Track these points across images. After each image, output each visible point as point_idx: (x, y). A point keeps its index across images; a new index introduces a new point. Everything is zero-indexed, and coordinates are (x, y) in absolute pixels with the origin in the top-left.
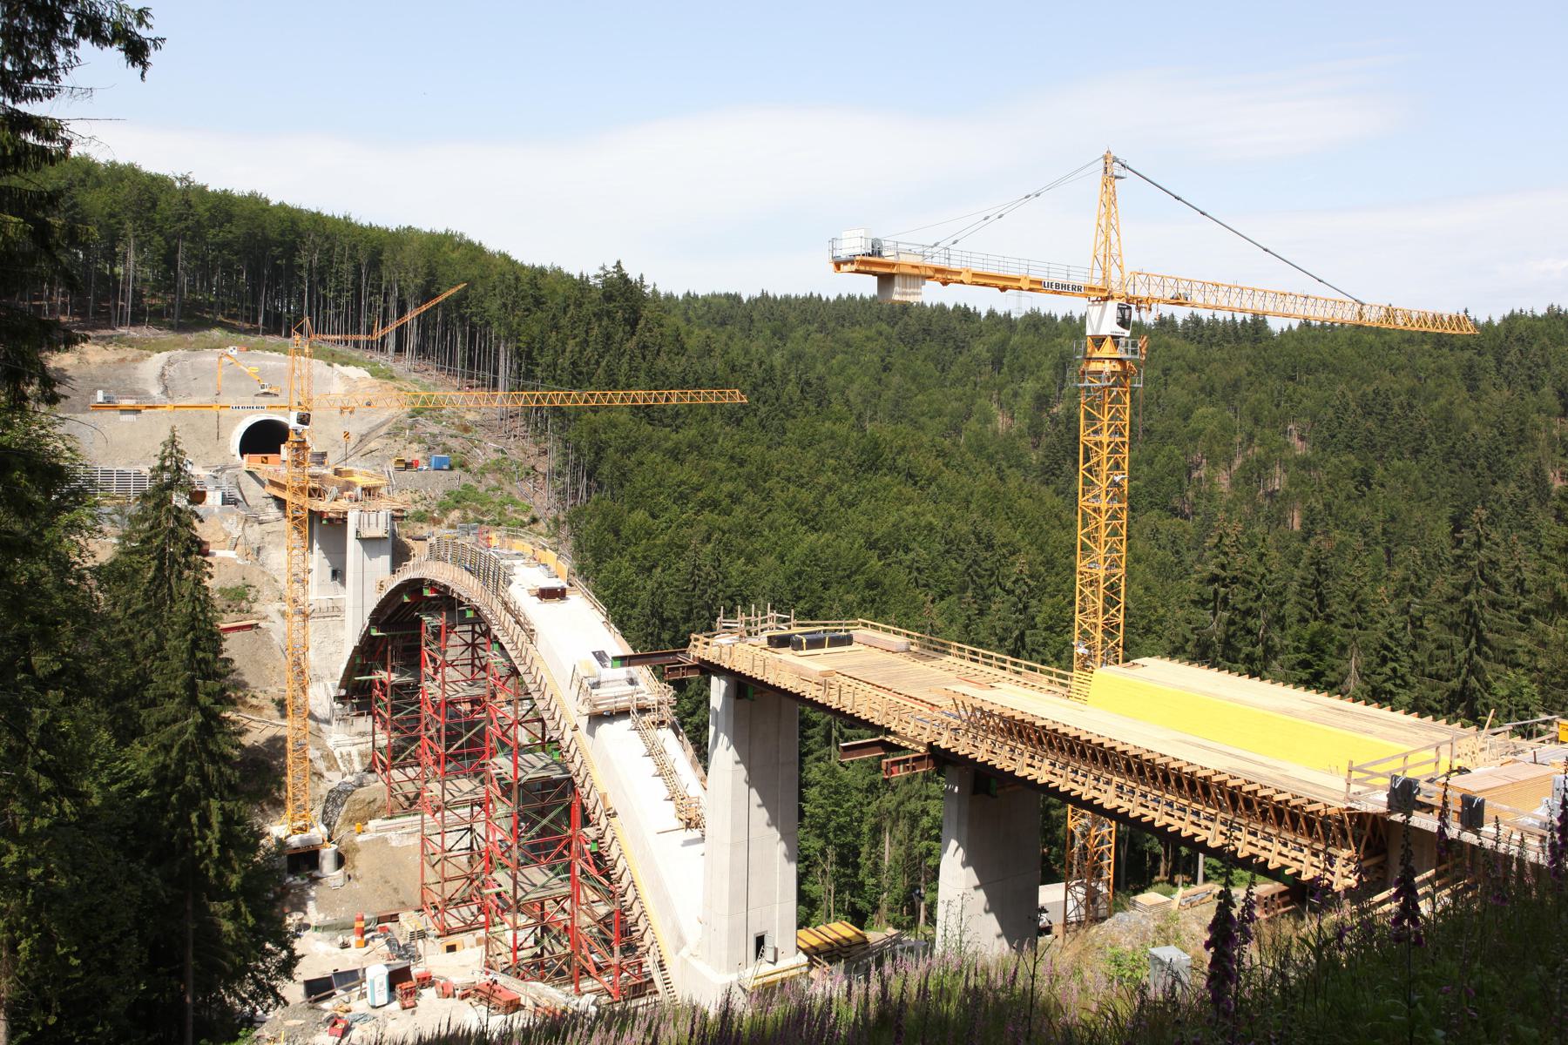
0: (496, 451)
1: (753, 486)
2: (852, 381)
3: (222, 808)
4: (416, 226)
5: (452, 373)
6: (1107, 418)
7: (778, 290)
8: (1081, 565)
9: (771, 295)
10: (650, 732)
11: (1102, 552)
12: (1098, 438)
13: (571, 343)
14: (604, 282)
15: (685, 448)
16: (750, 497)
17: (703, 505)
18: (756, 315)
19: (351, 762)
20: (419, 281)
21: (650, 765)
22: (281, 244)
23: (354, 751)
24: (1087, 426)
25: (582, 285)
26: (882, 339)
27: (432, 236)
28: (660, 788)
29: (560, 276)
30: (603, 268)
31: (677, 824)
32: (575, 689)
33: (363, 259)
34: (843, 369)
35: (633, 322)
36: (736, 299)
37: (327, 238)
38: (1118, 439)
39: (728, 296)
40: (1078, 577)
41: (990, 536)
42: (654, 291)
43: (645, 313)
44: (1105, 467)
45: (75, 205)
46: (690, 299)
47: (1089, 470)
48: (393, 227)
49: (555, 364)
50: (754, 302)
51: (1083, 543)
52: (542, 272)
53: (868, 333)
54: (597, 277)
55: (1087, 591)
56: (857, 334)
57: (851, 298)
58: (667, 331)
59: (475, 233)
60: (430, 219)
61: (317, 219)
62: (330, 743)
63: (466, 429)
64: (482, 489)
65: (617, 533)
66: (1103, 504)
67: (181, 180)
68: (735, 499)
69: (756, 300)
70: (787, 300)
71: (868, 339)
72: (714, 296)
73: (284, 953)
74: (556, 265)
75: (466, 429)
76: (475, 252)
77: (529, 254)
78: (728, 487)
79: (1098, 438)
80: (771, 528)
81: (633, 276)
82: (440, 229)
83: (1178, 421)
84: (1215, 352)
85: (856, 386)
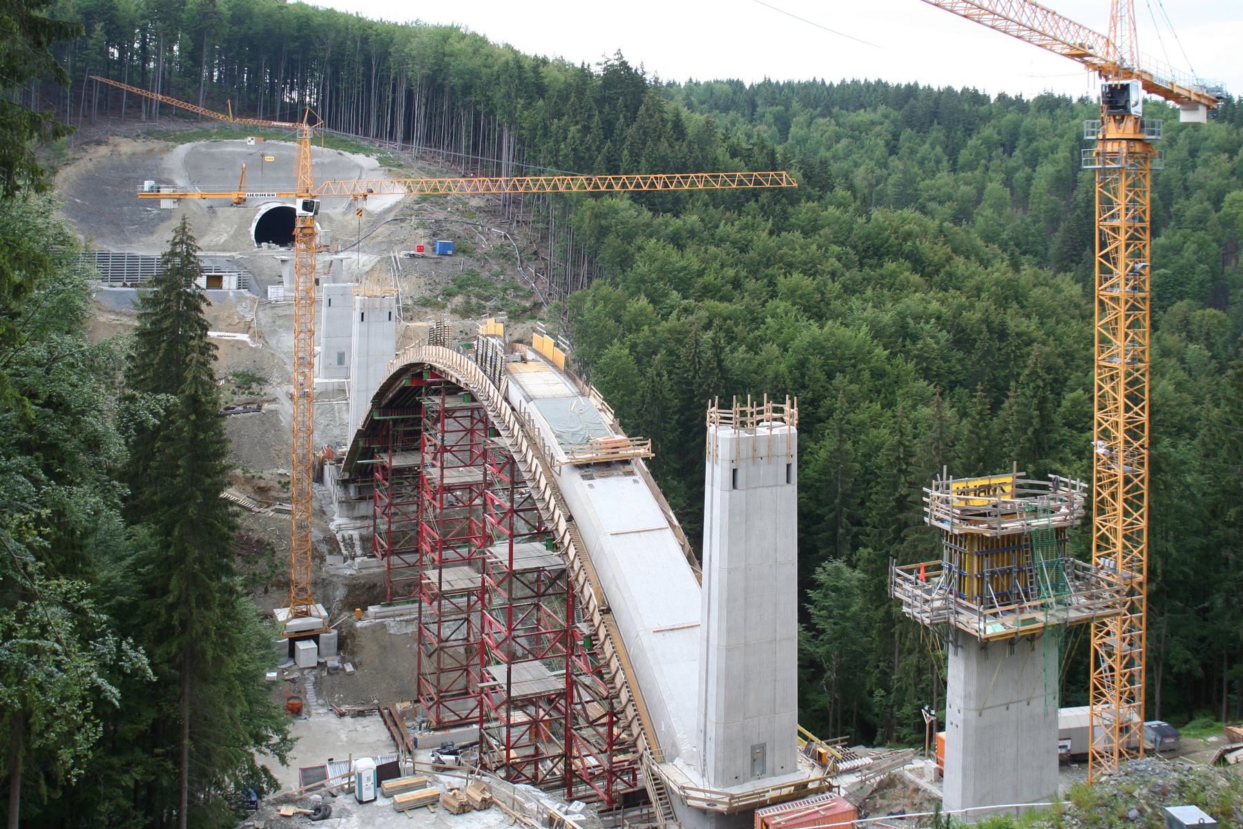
8: (1099, 359)
9: (774, 81)
15: (684, 234)
19: (352, 546)
20: (425, 71)
36: (737, 85)
38: (1138, 225)
39: (730, 82)
43: (646, 99)
46: (692, 86)
50: (757, 90)
56: (863, 116)
65: (618, 320)
68: (736, 284)
72: (716, 82)
78: (731, 272)
81: (633, 64)
85: (862, 169)
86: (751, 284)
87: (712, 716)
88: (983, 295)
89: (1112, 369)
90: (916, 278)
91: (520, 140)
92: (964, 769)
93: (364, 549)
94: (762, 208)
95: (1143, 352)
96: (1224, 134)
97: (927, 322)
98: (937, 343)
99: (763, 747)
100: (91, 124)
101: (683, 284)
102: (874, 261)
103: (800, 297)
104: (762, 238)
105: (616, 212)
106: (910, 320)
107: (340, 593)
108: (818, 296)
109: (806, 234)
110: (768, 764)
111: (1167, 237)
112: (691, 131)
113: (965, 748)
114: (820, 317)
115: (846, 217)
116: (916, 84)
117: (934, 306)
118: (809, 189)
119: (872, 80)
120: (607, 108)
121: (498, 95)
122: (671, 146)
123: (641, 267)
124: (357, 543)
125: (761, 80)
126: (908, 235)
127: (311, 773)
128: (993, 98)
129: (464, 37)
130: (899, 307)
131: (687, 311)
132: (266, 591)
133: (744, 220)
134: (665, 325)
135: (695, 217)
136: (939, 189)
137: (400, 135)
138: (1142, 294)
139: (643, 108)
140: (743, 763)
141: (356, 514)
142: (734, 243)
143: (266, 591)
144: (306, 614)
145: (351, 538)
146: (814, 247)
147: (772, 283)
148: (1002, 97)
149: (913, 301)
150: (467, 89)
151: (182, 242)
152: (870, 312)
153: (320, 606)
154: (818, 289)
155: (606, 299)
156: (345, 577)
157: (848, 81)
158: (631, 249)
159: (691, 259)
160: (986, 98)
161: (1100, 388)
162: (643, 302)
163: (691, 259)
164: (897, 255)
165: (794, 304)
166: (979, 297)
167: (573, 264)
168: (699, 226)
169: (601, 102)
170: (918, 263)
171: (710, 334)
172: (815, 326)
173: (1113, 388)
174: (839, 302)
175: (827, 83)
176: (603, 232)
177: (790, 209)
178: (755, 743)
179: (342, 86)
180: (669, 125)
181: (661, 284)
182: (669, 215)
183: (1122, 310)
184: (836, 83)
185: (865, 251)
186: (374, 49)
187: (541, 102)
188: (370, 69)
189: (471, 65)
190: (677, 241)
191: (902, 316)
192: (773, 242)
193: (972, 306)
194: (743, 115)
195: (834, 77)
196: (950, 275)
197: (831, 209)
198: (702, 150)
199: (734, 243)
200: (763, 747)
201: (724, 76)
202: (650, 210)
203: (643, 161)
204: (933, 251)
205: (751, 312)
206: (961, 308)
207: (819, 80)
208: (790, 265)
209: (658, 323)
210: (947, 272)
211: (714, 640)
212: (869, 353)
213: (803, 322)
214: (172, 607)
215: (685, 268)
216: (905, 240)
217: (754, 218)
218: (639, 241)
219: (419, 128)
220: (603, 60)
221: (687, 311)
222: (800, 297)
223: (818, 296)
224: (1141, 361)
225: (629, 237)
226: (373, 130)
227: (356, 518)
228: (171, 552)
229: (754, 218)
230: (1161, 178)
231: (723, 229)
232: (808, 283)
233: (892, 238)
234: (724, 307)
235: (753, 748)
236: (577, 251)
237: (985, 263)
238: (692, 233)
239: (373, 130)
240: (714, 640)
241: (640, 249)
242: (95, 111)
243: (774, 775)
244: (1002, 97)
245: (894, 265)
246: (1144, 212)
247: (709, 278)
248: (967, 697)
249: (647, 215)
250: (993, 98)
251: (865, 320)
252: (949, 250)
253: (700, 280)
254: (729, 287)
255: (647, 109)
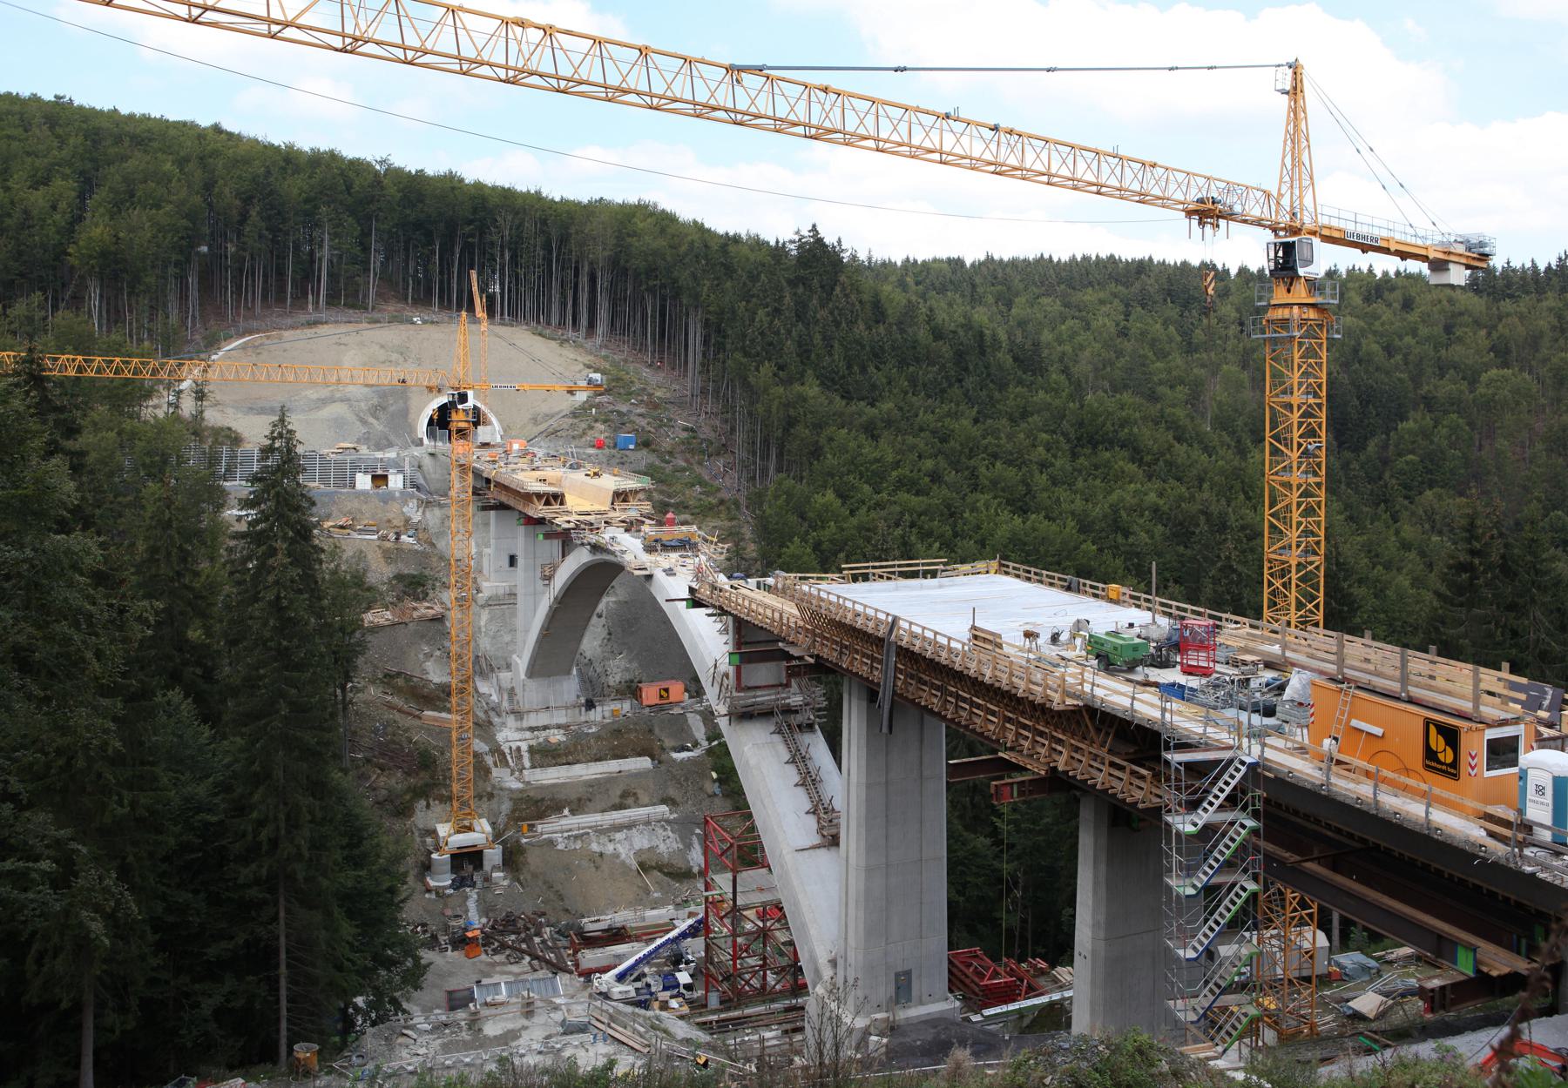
0: (686, 429)
1: (956, 465)
2: (1082, 348)
3: (1341, 916)
4: (608, 197)
5: (643, 349)
6: (1297, 374)
7: (1004, 253)
8: (1269, 551)
9: (996, 257)
10: (798, 736)
11: (1293, 535)
12: (1286, 399)
13: (761, 313)
14: (799, 248)
15: (880, 425)
16: (951, 477)
17: (901, 484)
18: (978, 280)
19: (520, 757)
20: (607, 253)
21: (792, 774)
22: (470, 222)
23: (524, 746)
24: (1274, 386)
25: (779, 251)
26: (1116, 302)
27: (623, 206)
28: (802, 801)
29: (758, 244)
30: (797, 233)
31: (817, 840)
32: (717, 686)
33: (554, 233)
34: (1072, 337)
35: (828, 289)
36: (957, 264)
37: (517, 213)
38: (1311, 401)
39: (949, 261)
40: (1266, 565)
41: (1223, 516)
42: (854, 258)
43: (843, 278)
44: (1296, 434)
45: (271, 193)
46: (909, 265)
47: (1276, 438)
48: (585, 201)
49: (744, 336)
50: (978, 267)
51: (1272, 526)
52: (736, 239)
53: (1102, 295)
54: (792, 242)
55: (1278, 584)
56: (1089, 296)
57: (1086, 259)
58: (865, 297)
59: (666, 202)
60: (622, 192)
61: (507, 194)
62: (500, 737)
63: (656, 407)
64: (669, 468)
65: (803, 517)
66: (1296, 477)
67: (381, 163)
68: (935, 477)
69: (981, 264)
70: (1014, 263)
71: (1102, 302)
72: (935, 260)
73: (409, 963)
74: (753, 233)
75: (656, 407)
76: (665, 221)
77: (722, 222)
78: (929, 464)
79: (1286, 399)
80: (972, 511)
81: (829, 239)
82: (632, 199)
83: (1464, 386)
84: (1507, 305)
85: (1087, 353)
86: (951, 477)
87: (852, 942)
88: (1206, 486)
89: (1283, 562)
90: (1132, 468)
91: (707, 324)
92: (1092, 1003)
93: (532, 759)
94: (966, 395)
95: (1318, 543)
96: (1483, 308)
97: (1142, 516)
98: (1152, 537)
99: (908, 973)
100: (254, 317)
101: (877, 479)
102: (1087, 451)
103: (1003, 490)
104: (964, 425)
105: (805, 400)
106: (1123, 514)
107: (506, 807)
108: (1022, 489)
109: (1012, 420)
110: (915, 993)
111: (1415, 421)
112: (892, 313)
113: (1093, 983)
114: (1024, 511)
115: (1057, 402)
116: (1150, 259)
117: (1152, 497)
118: (1019, 373)
119: (1103, 255)
120: (800, 290)
121: (684, 277)
122: (869, 328)
123: (830, 460)
124: (526, 756)
125: (982, 258)
126: (1124, 423)
127: (458, 995)
128: (1233, 272)
129: (652, 214)
130: (1114, 497)
131: (879, 505)
132: (428, 806)
133: (946, 408)
134: (854, 521)
135: (891, 405)
136: (1169, 372)
137: (584, 321)
138: (1318, 480)
139: (838, 289)
140: (885, 990)
141: (525, 724)
142: (933, 432)
143: (428, 806)
144: (470, 829)
145: (519, 749)
146: (1022, 436)
147: (974, 475)
148: (1243, 271)
149: (1125, 494)
150: (651, 271)
151: (281, 436)
152: (1079, 504)
153: (484, 822)
154: (1024, 482)
155: (789, 494)
156: (510, 790)
157: (1046, 256)
158: (822, 441)
159: (886, 449)
160: (1226, 272)
161: (1270, 584)
162: (830, 495)
163: (886, 449)
164: (1110, 443)
165: (995, 497)
166: (1200, 488)
167: (762, 458)
168: (897, 414)
169: (792, 283)
170: (1136, 453)
171: (898, 532)
172: (1018, 520)
173: (1284, 585)
174: (1045, 495)
175: (1055, 260)
176: (791, 423)
177: (997, 395)
178: (900, 969)
179: (521, 272)
180: (868, 306)
181: (851, 477)
182: (862, 403)
183: (1295, 497)
184: (1065, 258)
185: (1079, 439)
186: (554, 233)
187: (729, 284)
188: (550, 252)
189: (655, 245)
190: (871, 431)
191: (1115, 509)
192: (976, 431)
193: (1192, 498)
194: (963, 296)
195: (1061, 254)
196: (1169, 464)
197: (1041, 394)
198: (902, 331)
199: (933, 432)
200: (908, 973)
201: (943, 254)
202: (843, 397)
203: (836, 345)
204: (1148, 436)
205: (949, 507)
206: (1181, 498)
207: (1046, 256)
208: (995, 456)
209: (845, 519)
210: (1166, 462)
211: (853, 861)
212: (1076, 548)
213: (1005, 515)
214: (261, 823)
215: (877, 460)
216: (1122, 426)
217: (958, 405)
218: (830, 431)
219: (603, 314)
220: (797, 238)
221: (879, 505)
222: (1003, 490)
223: (1022, 489)
224: (1315, 553)
225: (818, 427)
226: (555, 320)
227: (522, 729)
228: (256, 767)
229: (958, 405)
230: (1411, 357)
231: (924, 418)
232: (1011, 474)
233: (1109, 424)
234: (915, 501)
235: (897, 975)
236: (766, 442)
237: (1208, 450)
238: (889, 423)
239: (555, 320)
240: (853, 861)
241: (831, 439)
242: (258, 302)
243: (921, 1003)
244: (1243, 271)
245: (1108, 455)
246: (1320, 386)
247: (905, 471)
248: (1095, 926)
249: (839, 403)
250: (1233, 272)
251: (1073, 513)
252: (1170, 437)
253: (894, 474)
254: (927, 479)
255: (843, 289)
